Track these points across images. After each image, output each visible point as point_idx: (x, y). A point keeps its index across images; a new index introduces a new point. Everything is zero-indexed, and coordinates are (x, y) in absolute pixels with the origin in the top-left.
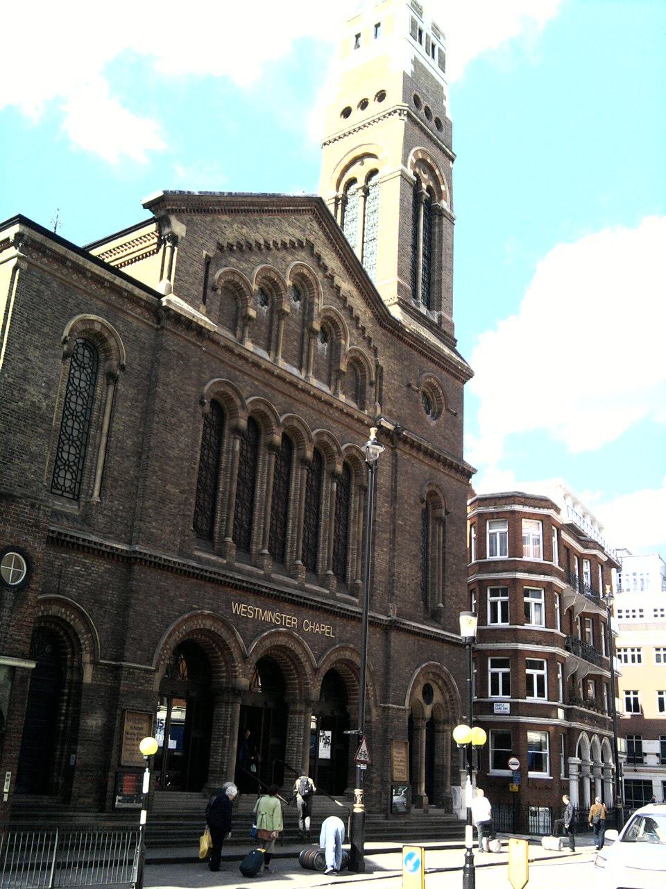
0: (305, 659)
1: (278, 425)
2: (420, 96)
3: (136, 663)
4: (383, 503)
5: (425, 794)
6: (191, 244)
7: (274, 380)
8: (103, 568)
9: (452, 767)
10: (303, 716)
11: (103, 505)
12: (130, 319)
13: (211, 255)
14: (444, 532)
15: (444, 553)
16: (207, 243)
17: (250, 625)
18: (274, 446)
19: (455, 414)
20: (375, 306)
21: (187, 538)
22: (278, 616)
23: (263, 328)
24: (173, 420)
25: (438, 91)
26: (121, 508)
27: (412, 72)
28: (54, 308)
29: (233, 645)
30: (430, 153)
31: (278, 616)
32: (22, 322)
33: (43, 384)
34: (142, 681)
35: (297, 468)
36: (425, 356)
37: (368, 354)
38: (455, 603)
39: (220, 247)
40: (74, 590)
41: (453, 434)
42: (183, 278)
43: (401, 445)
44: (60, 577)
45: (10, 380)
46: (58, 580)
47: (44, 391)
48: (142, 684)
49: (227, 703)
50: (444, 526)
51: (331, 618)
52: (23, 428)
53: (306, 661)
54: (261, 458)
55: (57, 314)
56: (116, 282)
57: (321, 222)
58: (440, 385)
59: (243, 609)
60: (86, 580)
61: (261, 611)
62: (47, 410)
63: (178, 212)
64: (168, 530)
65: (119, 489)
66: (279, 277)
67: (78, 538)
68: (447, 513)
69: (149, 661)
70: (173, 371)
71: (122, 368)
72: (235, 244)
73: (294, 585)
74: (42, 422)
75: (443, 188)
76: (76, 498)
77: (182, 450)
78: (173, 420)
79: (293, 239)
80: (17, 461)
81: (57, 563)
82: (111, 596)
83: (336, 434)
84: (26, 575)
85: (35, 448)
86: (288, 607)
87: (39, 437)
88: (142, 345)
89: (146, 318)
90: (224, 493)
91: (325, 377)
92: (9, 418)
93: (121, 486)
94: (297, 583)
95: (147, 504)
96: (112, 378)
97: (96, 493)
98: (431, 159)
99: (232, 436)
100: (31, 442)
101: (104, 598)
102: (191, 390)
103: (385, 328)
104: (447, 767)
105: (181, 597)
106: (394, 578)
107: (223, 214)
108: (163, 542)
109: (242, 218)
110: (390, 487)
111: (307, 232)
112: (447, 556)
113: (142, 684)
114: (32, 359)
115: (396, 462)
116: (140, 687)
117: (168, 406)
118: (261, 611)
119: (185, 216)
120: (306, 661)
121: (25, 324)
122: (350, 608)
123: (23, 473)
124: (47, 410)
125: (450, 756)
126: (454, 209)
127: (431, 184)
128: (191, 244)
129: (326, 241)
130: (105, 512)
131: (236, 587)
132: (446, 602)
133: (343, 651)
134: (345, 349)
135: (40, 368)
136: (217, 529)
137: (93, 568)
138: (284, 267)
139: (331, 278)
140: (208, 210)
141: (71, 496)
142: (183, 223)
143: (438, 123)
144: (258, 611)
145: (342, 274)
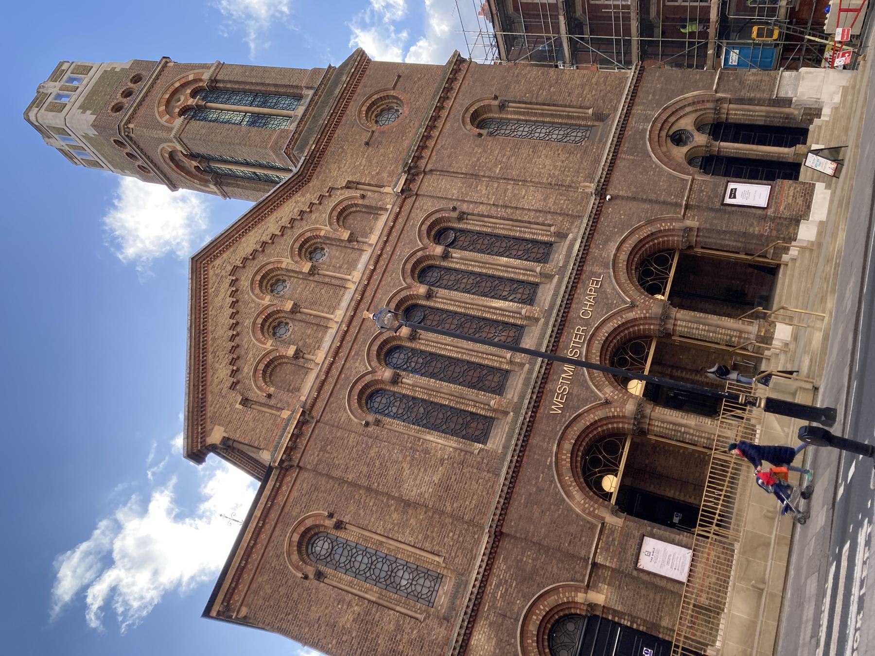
0: (619, 318)
1: (373, 372)
2: (113, 104)
3: (592, 544)
4: (477, 192)
5: (793, 149)
6: (230, 422)
7: (352, 329)
8: (502, 565)
9: (769, 105)
10: (679, 323)
11: (447, 556)
12: (291, 499)
13: (240, 398)
14: (515, 102)
15: (537, 104)
16: (230, 402)
17: (575, 391)
18: (411, 335)
19: (399, 77)
20: (290, 189)
21: (485, 461)
22: (571, 352)
23: (309, 331)
24: (377, 464)
25: (108, 76)
26: (451, 534)
27: (91, 114)
28: (279, 583)
29: (592, 416)
30: (159, 96)
31: (571, 352)
32: (288, 622)
33: (340, 606)
34: (611, 539)
35: (436, 302)
36: (340, 119)
37: (330, 204)
38: (590, 91)
39: (233, 386)
40: (518, 602)
41: (419, 79)
42: (258, 435)
43: (422, 163)
44: (504, 616)
45: (334, 642)
46: (507, 619)
47: (345, 607)
48: (614, 540)
49: (675, 325)
50: (509, 102)
51: (583, 277)
52: (374, 636)
53: (622, 318)
54: (423, 348)
55: (284, 582)
56: (259, 515)
57: (214, 256)
58: (369, 97)
59: (559, 400)
60: (511, 586)
61: (563, 375)
62: (361, 606)
63: (204, 434)
64: (474, 486)
65: (434, 535)
66: (261, 312)
67: (472, 593)
68: (496, 98)
69: (593, 527)
70: (335, 459)
71: (331, 516)
72: (231, 367)
73: (648, 13)
74: (370, 614)
75: (191, 77)
76: (439, 578)
77: (405, 457)
78: (377, 464)
79: (229, 293)
80: (401, 647)
81: (492, 617)
82: (528, 558)
83: (407, 252)
84: (647, 150)
85: (391, 626)
86: (564, 338)
87: (383, 619)
88: (313, 488)
89: (291, 481)
90: (451, 400)
91: (355, 255)
92: (365, 649)
93: (432, 532)
94: (543, 319)
95: (449, 509)
96: (339, 525)
97: (437, 559)
98: (165, 93)
99: (400, 384)
100: (386, 628)
101: (529, 568)
102: (352, 439)
103: (311, 176)
104: (767, 112)
105: (537, 478)
106: (553, 183)
107: (366, 56)
108: (484, 493)
109: (210, 356)
110: (464, 180)
111: (223, 273)
112: (540, 100)
113: (614, 540)
114: (318, 615)
115: (436, 170)
116: (616, 543)
117: (365, 469)
118: (563, 375)
119: (209, 425)
120: (622, 318)
121: (290, 617)
122: (629, 85)
123: (411, 643)
124: (361, 606)
125: (757, 108)
126: (209, 61)
127: (189, 91)
128: (230, 422)
129: (231, 249)
130: (453, 554)
131: (536, 406)
132: (588, 104)
133: (618, 263)
134: (329, 232)
135: (327, 608)
136: (482, 412)
137: (501, 577)
138: (253, 305)
139: (264, 244)
140: (202, 399)
141: (589, 132)
142: (213, 429)
143: (137, 79)
144: (563, 378)
145: (260, 231)
